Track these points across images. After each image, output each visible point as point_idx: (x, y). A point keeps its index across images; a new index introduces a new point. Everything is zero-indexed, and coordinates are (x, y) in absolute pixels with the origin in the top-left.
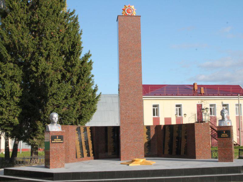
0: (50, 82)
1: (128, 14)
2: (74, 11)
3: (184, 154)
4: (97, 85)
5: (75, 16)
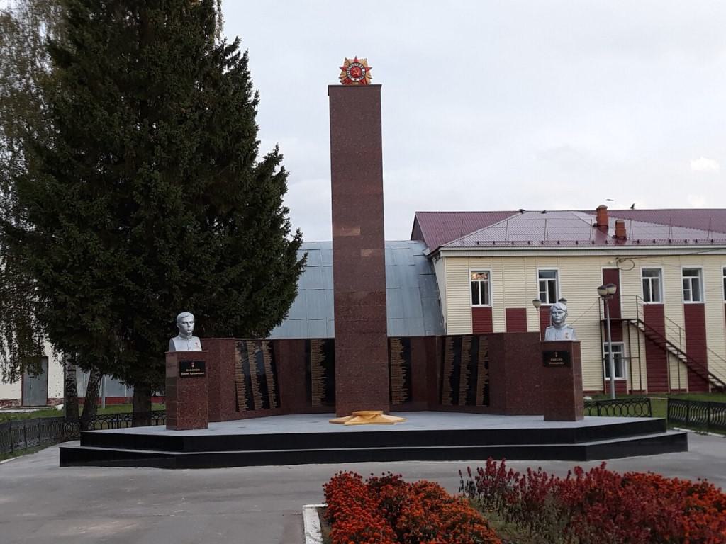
0: (178, 232)
1: (353, 79)
2: (237, 40)
3: (484, 404)
4: (301, 232)
5: (239, 53)
